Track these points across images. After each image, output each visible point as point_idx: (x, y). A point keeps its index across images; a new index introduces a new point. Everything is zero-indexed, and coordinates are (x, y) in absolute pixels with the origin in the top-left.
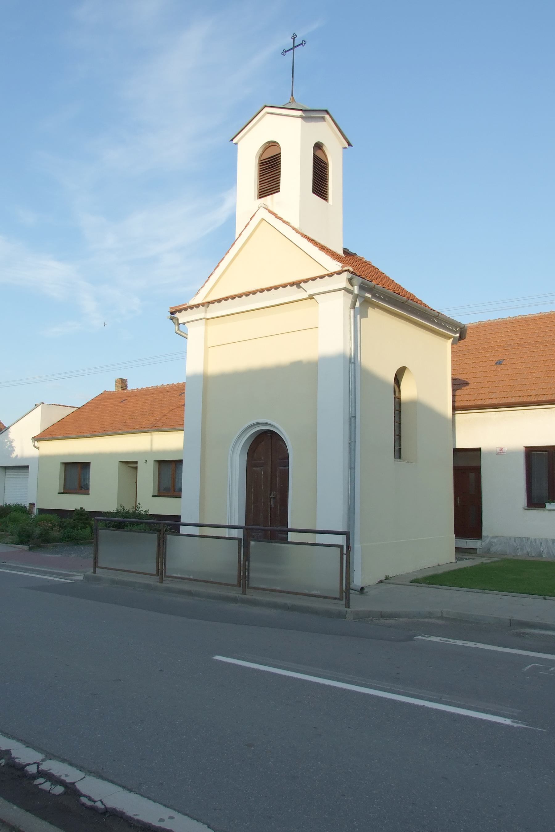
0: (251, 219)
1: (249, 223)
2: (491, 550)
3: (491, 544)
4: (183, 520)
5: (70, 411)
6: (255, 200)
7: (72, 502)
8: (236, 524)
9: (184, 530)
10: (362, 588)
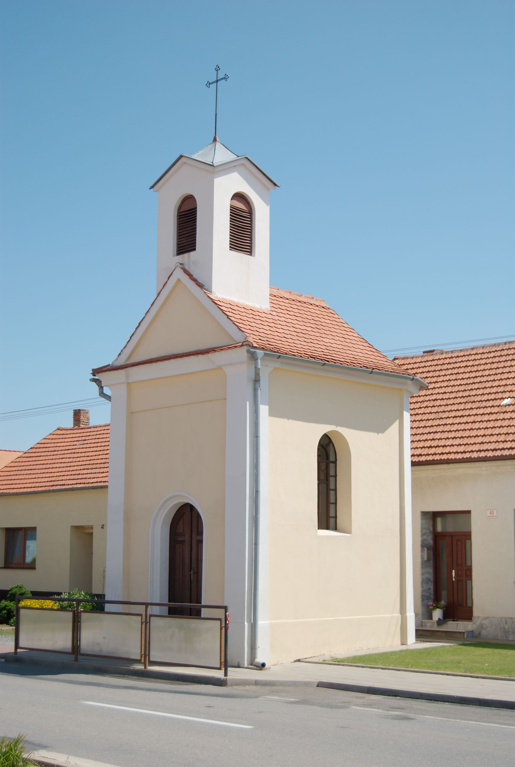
0: (169, 278)
1: (166, 282)
2: (482, 634)
3: (481, 626)
4: (107, 599)
5: (13, 456)
6: (174, 256)
7: (404, 647)
8: (158, 602)
9: (108, 607)
10: (263, 665)
